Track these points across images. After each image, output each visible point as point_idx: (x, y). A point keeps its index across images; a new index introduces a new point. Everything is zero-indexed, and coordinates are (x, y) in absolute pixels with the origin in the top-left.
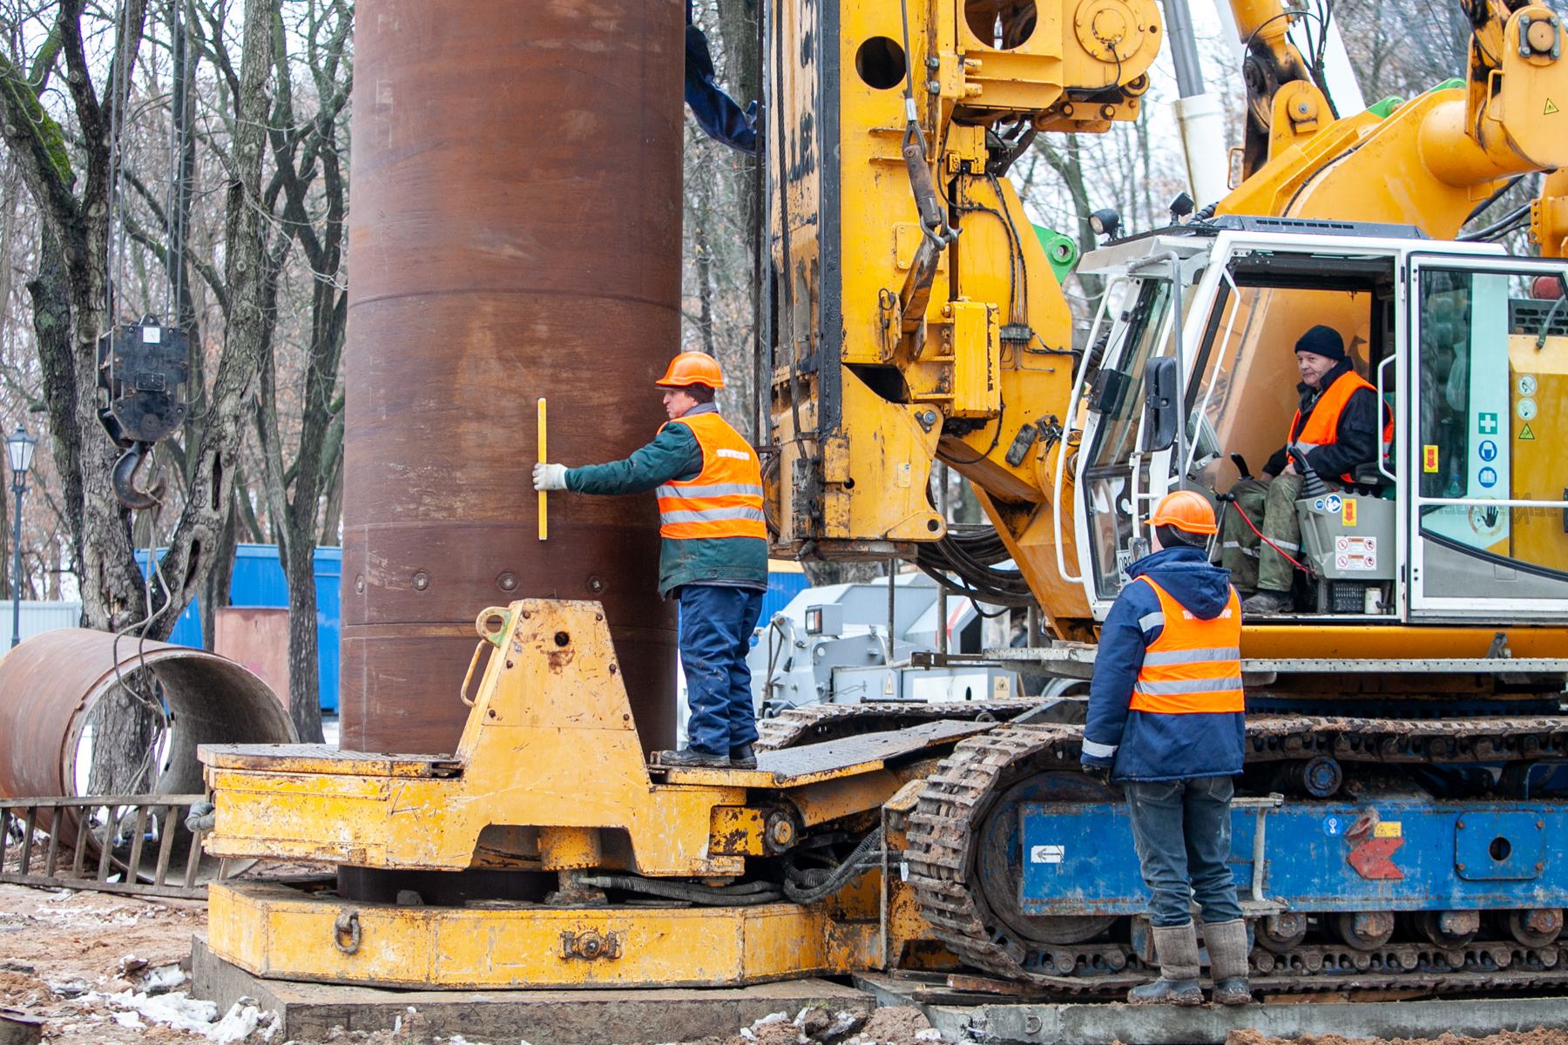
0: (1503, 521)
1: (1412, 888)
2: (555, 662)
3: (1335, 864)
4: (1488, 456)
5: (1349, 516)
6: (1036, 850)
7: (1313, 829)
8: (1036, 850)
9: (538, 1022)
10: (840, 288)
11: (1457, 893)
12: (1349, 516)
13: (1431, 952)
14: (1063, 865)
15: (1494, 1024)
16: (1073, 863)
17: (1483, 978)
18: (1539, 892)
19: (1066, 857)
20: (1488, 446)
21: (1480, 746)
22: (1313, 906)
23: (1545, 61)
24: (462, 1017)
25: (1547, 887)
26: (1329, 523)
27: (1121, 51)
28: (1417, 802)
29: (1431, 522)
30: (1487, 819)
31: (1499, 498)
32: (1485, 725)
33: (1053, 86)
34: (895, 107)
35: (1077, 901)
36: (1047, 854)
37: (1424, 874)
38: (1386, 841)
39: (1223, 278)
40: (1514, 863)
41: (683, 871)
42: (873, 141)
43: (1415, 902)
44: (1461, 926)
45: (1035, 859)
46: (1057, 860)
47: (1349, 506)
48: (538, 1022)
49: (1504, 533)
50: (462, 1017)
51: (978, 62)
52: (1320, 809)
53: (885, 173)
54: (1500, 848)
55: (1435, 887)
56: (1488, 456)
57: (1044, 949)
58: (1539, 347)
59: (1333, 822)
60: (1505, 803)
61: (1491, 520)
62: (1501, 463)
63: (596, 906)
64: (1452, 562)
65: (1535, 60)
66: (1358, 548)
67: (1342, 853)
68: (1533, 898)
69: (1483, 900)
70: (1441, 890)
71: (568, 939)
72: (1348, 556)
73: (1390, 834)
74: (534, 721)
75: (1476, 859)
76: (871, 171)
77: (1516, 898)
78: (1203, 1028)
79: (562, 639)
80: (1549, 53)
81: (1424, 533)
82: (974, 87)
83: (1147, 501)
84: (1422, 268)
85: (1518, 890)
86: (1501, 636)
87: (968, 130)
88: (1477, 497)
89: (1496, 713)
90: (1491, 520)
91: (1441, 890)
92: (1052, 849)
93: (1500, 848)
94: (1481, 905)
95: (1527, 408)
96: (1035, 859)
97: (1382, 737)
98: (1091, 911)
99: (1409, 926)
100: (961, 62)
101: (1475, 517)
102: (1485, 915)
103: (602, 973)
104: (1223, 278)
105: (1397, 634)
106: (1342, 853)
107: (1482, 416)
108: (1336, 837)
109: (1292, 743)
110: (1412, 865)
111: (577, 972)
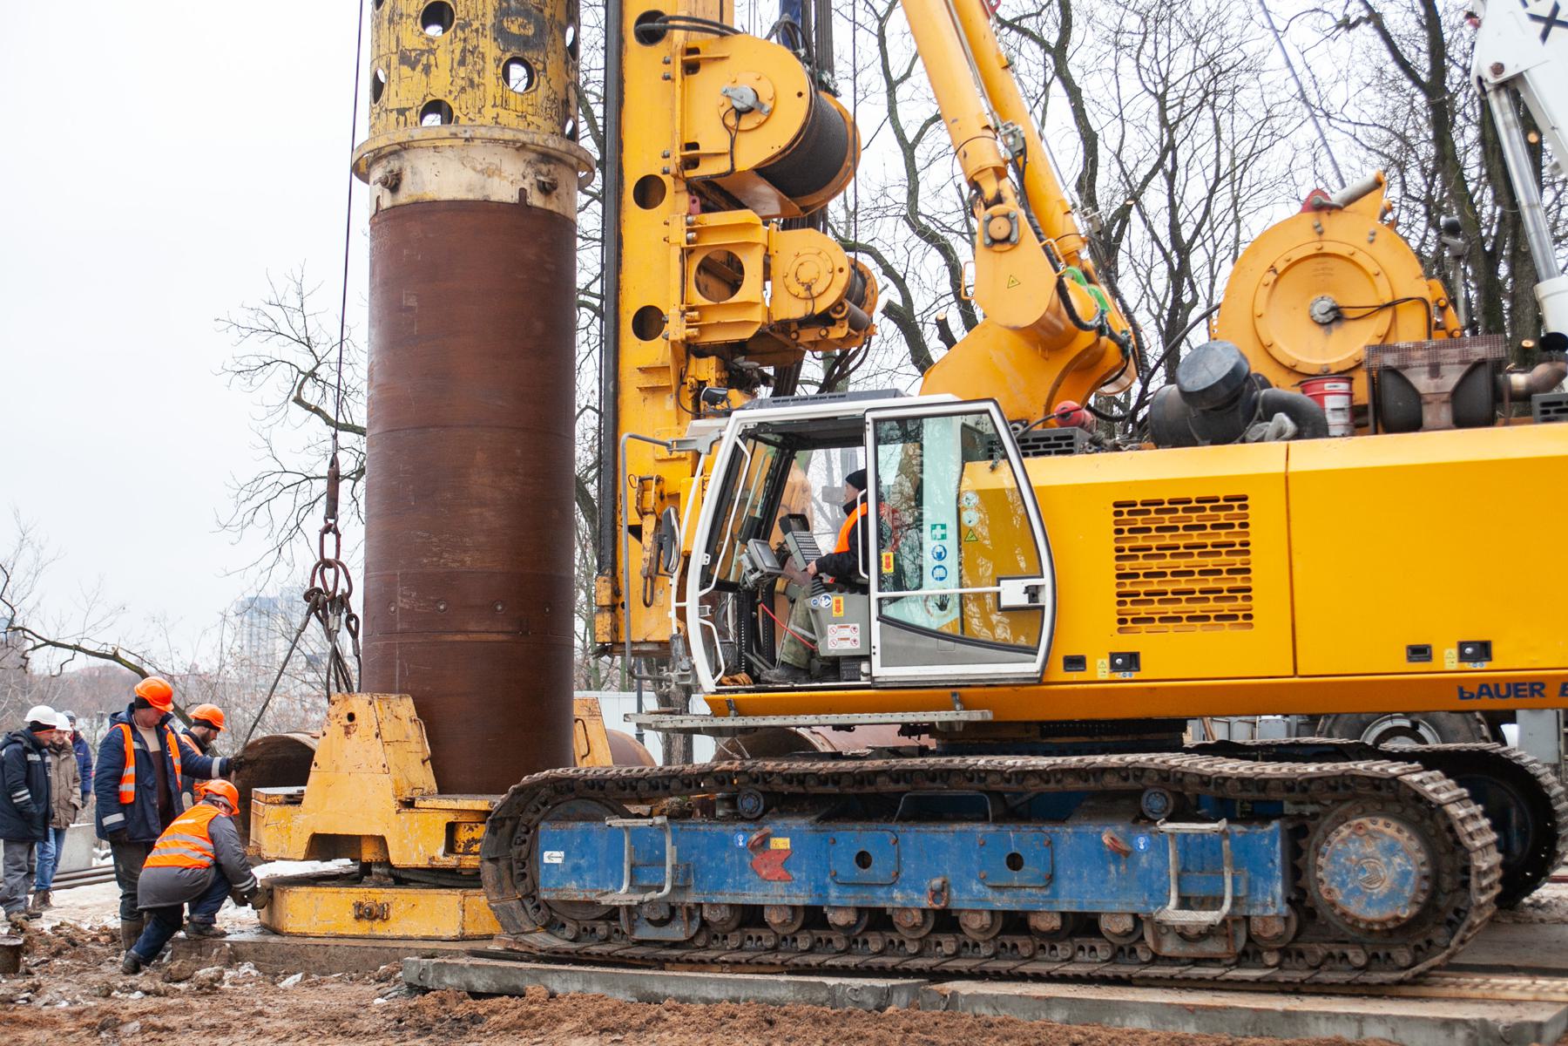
0: (953, 606)
1: (799, 888)
2: (347, 733)
3: (743, 868)
4: (940, 557)
5: (838, 609)
6: (546, 854)
7: (725, 843)
8: (546, 854)
9: (293, 956)
10: (1175, 446)
11: (833, 893)
12: (838, 609)
13: (1421, 942)
14: (563, 865)
15: (722, 995)
16: (569, 864)
17: (1011, 964)
18: (897, 894)
19: (566, 858)
20: (940, 549)
21: (880, 779)
22: (729, 899)
23: (1007, 246)
24: (256, 951)
25: (903, 890)
26: (822, 615)
27: (816, 290)
28: (799, 824)
29: (890, 611)
30: (855, 836)
31: (951, 588)
32: (1114, 759)
33: (755, 323)
34: (655, 351)
35: (574, 890)
36: (553, 857)
37: (808, 878)
38: (779, 851)
39: (736, 445)
40: (877, 871)
41: (423, 863)
42: (642, 376)
43: (802, 899)
44: (839, 918)
45: (546, 860)
46: (559, 861)
47: (838, 602)
48: (293, 956)
49: (956, 614)
50: (256, 951)
51: (696, 314)
52: (731, 828)
53: (649, 396)
54: (863, 860)
55: (817, 887)
56: (940, 557)
57: (561, 919)
58: (993, 468)
59: (741, 838)
60: (867, 825)
61: (943, 607)
62: (951, 561)
63: (389, 886)
64: (902, 639)
65: (998, 247)
66: (846, 633)
67: (748, 860)
68: (892, 899)
69: (854, 899)
70: (821, 889)
71: (359, 906)
72: (838, 640)
73: (782, 847)
74: (337, 769)
75: (846, 866)
76: (641, 396)
77: (879, 898)
78: (519, 983)
79: (351, 717)
80: (1007, 239)
81: (882, 618)
82: (694, 332)
83: (684, 609)
84: (876, 421)
85: (881, 892)
86: (954, 694)
87: (704, 361)
88: (932, 587)
89: (1047, 754)
90: (943, 607)
91: (821, 889)
92: (556, 854)
93: (863, 860)
94: (852, 903)
95: (971, 517)
96: (546, 860)
97: (1103, 771)
98: (581, 897)
99: (813, 917)
100: (683, 314)
101: (931, 604)
102: (860, 911)
103: (379, 929)
104: (736, 445)
105: (875, 696)
106: (748, 860)
107: (934, 527)
108: (742, 849)
109: (991, 779)
110: (798, 869)
111: (363, 928)
